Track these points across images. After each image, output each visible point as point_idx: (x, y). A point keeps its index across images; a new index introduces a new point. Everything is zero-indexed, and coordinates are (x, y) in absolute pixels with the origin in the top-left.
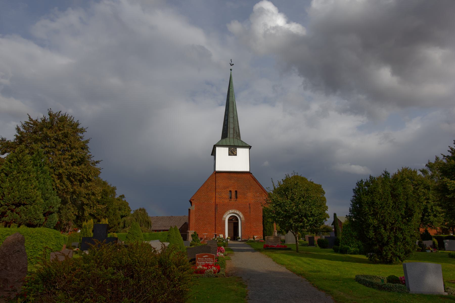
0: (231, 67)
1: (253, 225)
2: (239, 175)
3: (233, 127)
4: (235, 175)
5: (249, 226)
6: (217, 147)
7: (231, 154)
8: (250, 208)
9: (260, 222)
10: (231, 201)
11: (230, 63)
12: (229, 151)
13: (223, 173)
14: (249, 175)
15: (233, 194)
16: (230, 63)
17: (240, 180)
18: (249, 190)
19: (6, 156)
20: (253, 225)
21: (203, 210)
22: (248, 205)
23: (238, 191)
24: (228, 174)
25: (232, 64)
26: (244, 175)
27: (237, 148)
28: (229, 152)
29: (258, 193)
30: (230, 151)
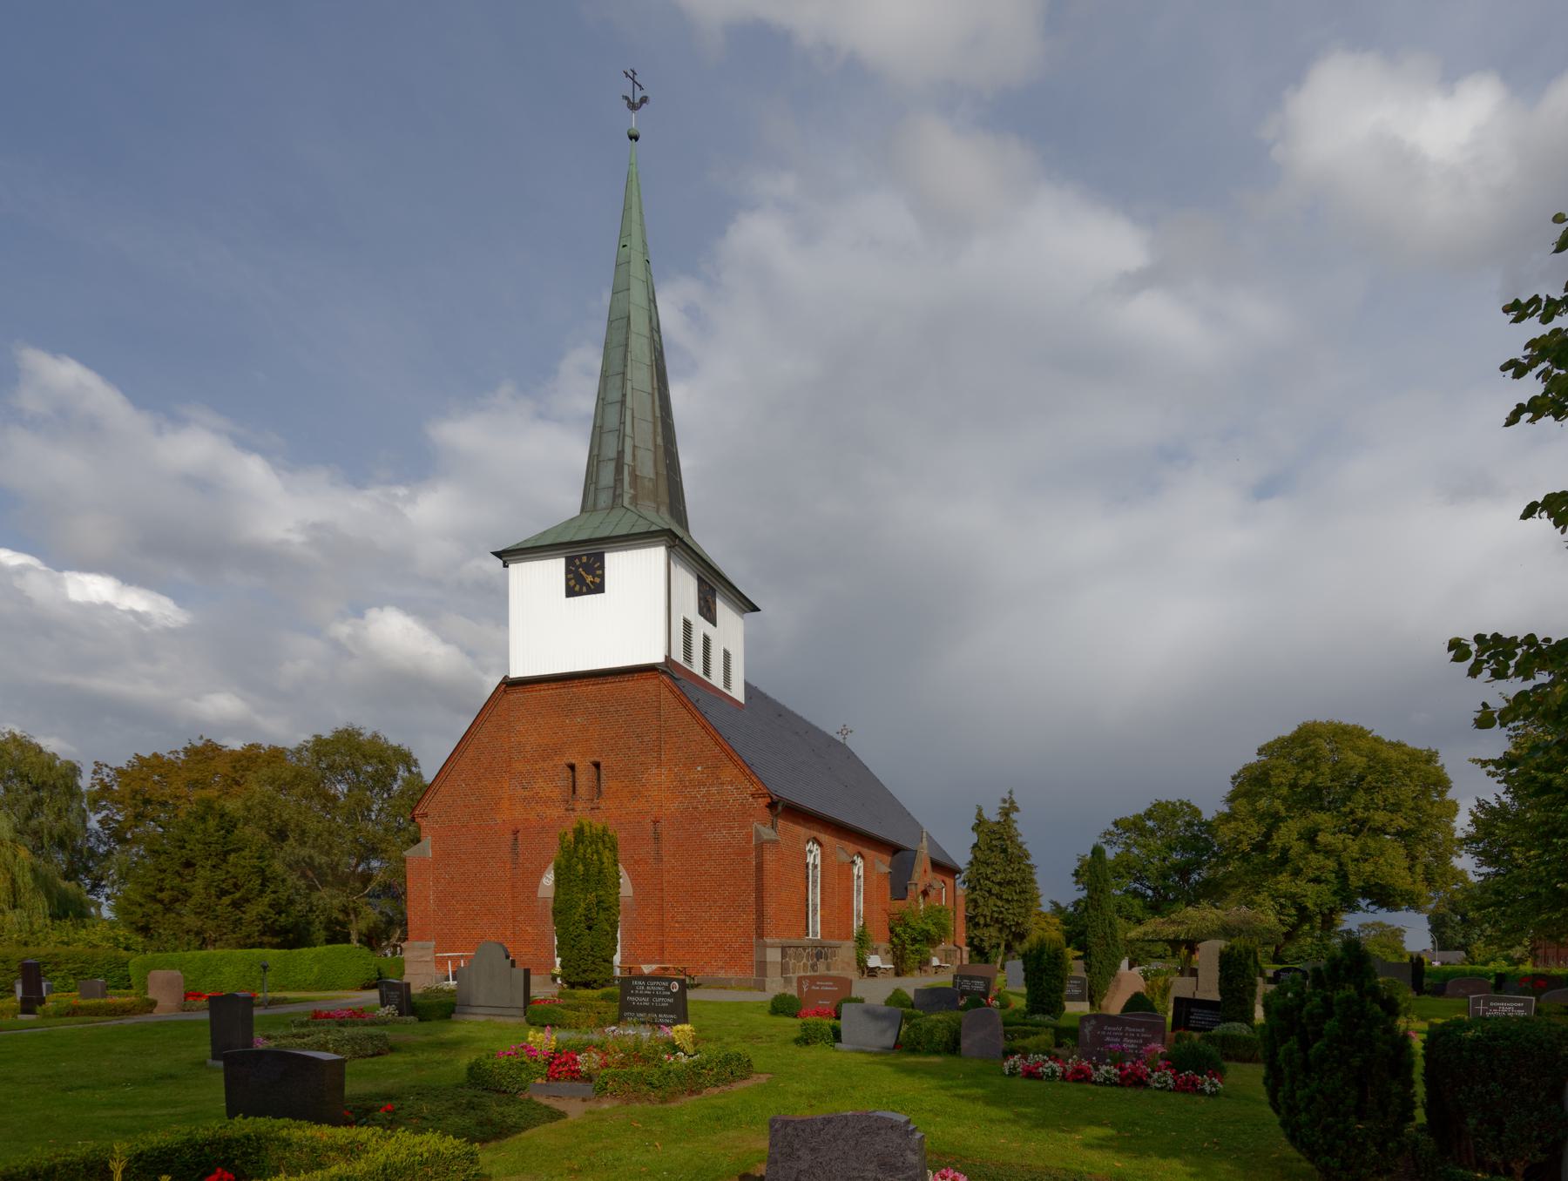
0: (634, 121)
2: (607, 687)
4: (590, 689)
5: (650, 920)
6: (608, 552)
7: (577, 588)
8: (657, 838)
9: (706, 900)
10: (573, 810)
12: (568, 571)
14: (656, 682)
15: (584, 778)
17: (612, 709)
20: (673, 917)
21: (463, 857)
22: (650, 827)
23: (602, 765)
24: (560, 684)
25: (637, 100)
28: (568, 580)
29: (699, 769)
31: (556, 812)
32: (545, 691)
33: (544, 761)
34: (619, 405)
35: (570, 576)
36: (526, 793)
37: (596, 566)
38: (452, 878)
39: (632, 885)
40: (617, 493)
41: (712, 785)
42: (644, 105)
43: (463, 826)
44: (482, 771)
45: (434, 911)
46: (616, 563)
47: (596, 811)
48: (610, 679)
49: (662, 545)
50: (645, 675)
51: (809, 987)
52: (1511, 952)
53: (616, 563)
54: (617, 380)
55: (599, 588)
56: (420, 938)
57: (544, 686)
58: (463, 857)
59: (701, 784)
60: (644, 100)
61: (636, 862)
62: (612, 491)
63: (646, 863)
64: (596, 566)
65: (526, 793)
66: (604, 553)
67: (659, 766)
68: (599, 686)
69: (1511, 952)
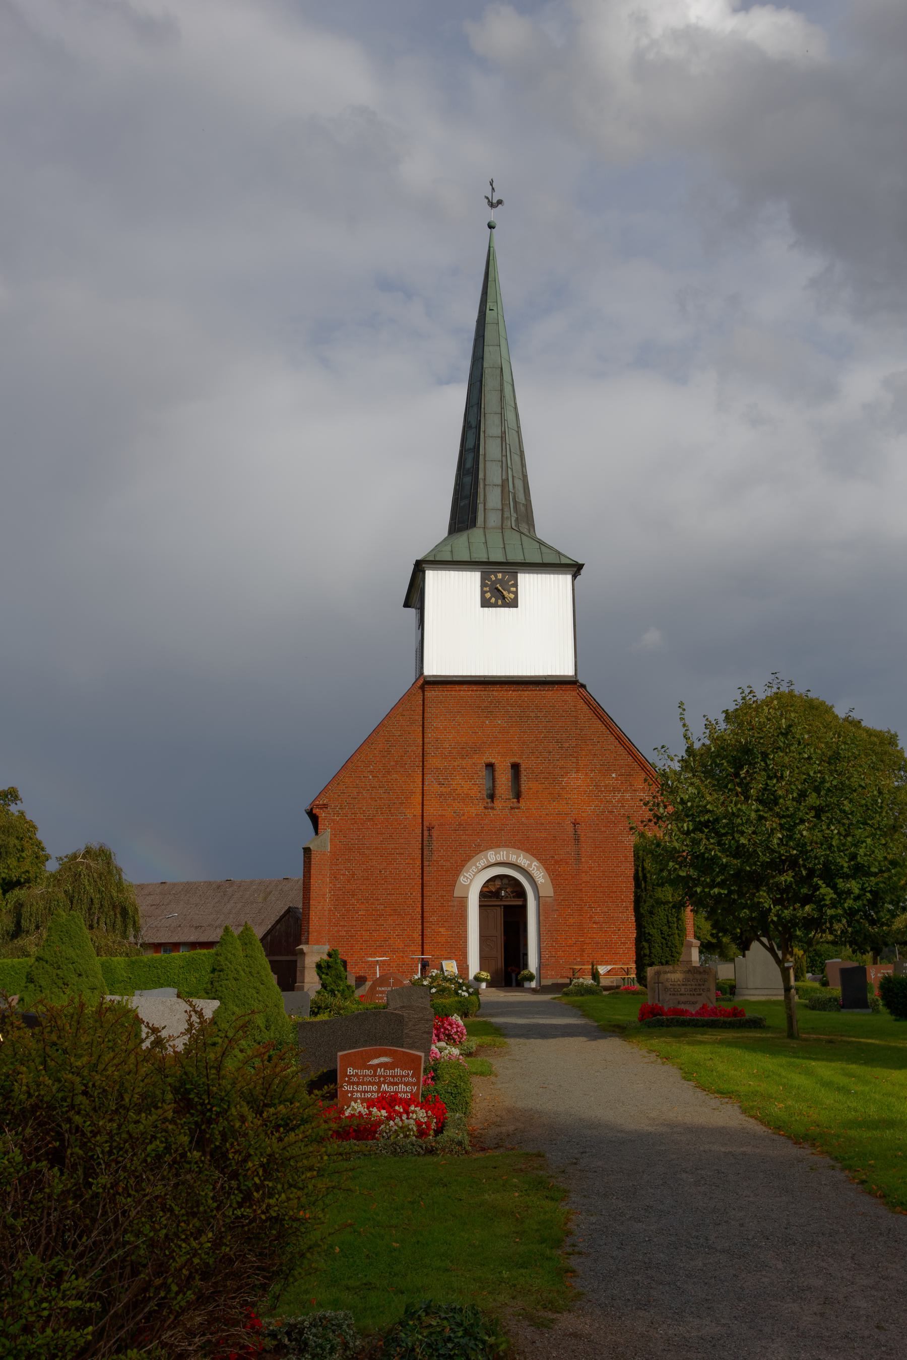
0: (493, 215)
1: (591, 917)
2: (527, 694)
3: (503, 481)
4: (511, 694)
5: (571, 921)
6: (521, 573)
7: (493, 600)
8: (577, 839)
9: (622, 901)
10: (492, 808)
11: (487, 198)
12: (483, 585)
13: (457, 687)
14: (574, 694)
15: (504, 779)
16: (487, 198)
17: (533, 715)
18: (574, 760)
19: (27, 817)
20: (591, 917)
21: (367, 852)
22: (570, 828)
23: (522, 768)
24: (480, 687)
25: (495, 201)
26: (549, 694)
27: (519, 576)
28: (483, 593)
29: (614, 775)
30: (487, 589)
31: (474, 809)
32: (464, 690)
33: (463, 758)
34: (499, 440)
35: (485, 589)
36: (443, 789)
37: (510, 583)
38: (354, 874)
39: (553, 885)
40: (505, 516)
41: (626, 791)
42: (500, 205)
43: (369, 820)
44: (392, 763)
45: (330, 910)
46: (528, 583)
47: (516, 810)
48: (531, 687)
49: (569, 574)
50: (564, 687)
51: (876, 975)
52: (262, 1026)
53: (528, 583)
54: (475, 409)
55: (514, 604)
56: (318, 942)
57: (465, 687)
58: (367, 852)
59: (615, 790)
60: (500, 202)
61: (557, 862)
62: (500, 513)
63: (567, 863)
64: (510, 583)
65: (443, 789)
66: (517, 572)
67: (577, 771)
68: (520, 692)
69: (262, 1026)
